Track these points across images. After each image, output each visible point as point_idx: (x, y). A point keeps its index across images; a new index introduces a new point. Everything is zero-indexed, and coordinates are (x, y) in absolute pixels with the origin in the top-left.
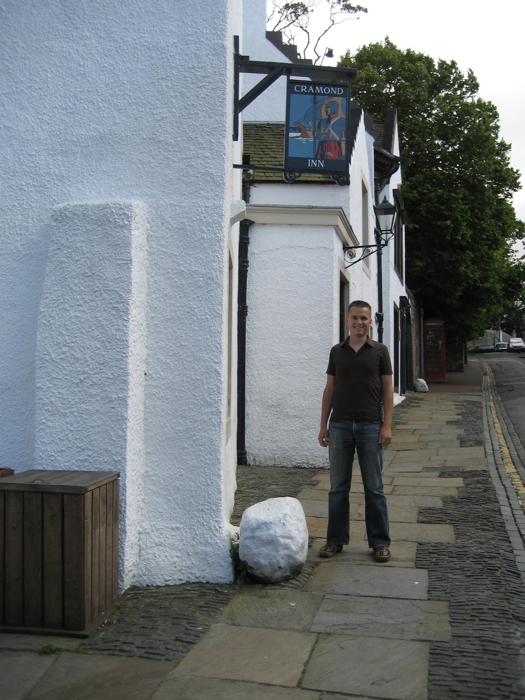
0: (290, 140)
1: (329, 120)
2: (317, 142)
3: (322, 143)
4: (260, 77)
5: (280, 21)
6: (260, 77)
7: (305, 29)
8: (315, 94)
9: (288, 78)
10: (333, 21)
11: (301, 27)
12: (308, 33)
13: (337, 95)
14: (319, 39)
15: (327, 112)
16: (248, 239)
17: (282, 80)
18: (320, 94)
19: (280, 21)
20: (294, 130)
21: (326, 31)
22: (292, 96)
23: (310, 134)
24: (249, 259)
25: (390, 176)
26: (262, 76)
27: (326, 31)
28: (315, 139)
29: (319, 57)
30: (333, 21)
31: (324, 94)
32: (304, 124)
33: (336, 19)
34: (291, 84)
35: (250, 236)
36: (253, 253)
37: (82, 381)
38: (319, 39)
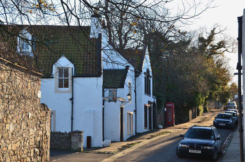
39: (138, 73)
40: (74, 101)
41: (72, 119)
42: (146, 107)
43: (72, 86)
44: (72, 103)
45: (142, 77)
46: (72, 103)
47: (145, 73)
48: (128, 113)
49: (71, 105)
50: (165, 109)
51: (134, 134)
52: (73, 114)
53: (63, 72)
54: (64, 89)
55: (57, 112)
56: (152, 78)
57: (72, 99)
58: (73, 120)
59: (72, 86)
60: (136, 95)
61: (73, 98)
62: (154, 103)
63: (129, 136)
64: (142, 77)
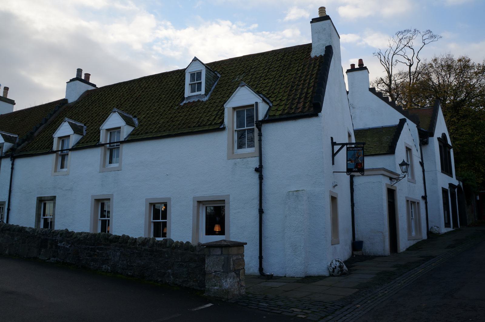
0: (348, 164)
1: (358, 157)
2: (355, 163)
3: (357, 164)
4: (340, 146)
5: (397, 48)
6: (340, 146)
7: (411, 47)
8: (354, 150)
9: (347, 146)
10: (424, 43)
11: (409, 47)
12: (413, 49)
13: (360, 150)
14: (418, 52)
15: (358, 155)
16: (353, 181)
17: (345, 147)
18: (355, 150)
19: (397, 48)
20: (349, 161)
21: (421, 48)
22: (348, 151)
23: (353, 161)
24: (354, 187)
25: (353, 187)
26: (335, 153)
27: (421, 48)
28: (355, 163)
29: (419, 61)
30: (424, 43)
31: (357, 150)
32: (351, 159)
33: (426, 42)
34: (347, 148)
35: (353, 180)
36: (355, 185)
37: (295, 231)
38: (418, 52)
39: (425, 136)
40: (265, 173)
41: (261, 211)
42: (444, 191)
43: (260, 140)
44: (261, 178)
45: (434, 143)
46: (261, 178)
47: (439, 139)
48: (202, 70)
49: (257, 181)
50: (478, 198)
51: (424, 236)
52: (263, 201)
53: (246, 113)
54: (246, 150)
55: (231, 198)
56: (452, 150)
57: (259, 170)
58: (264, 215)
59: (260, 140)
60: (420, 50)
61: (261, 166)
62: (459, 187)
63: (412, 243)
64: (434, 143)
